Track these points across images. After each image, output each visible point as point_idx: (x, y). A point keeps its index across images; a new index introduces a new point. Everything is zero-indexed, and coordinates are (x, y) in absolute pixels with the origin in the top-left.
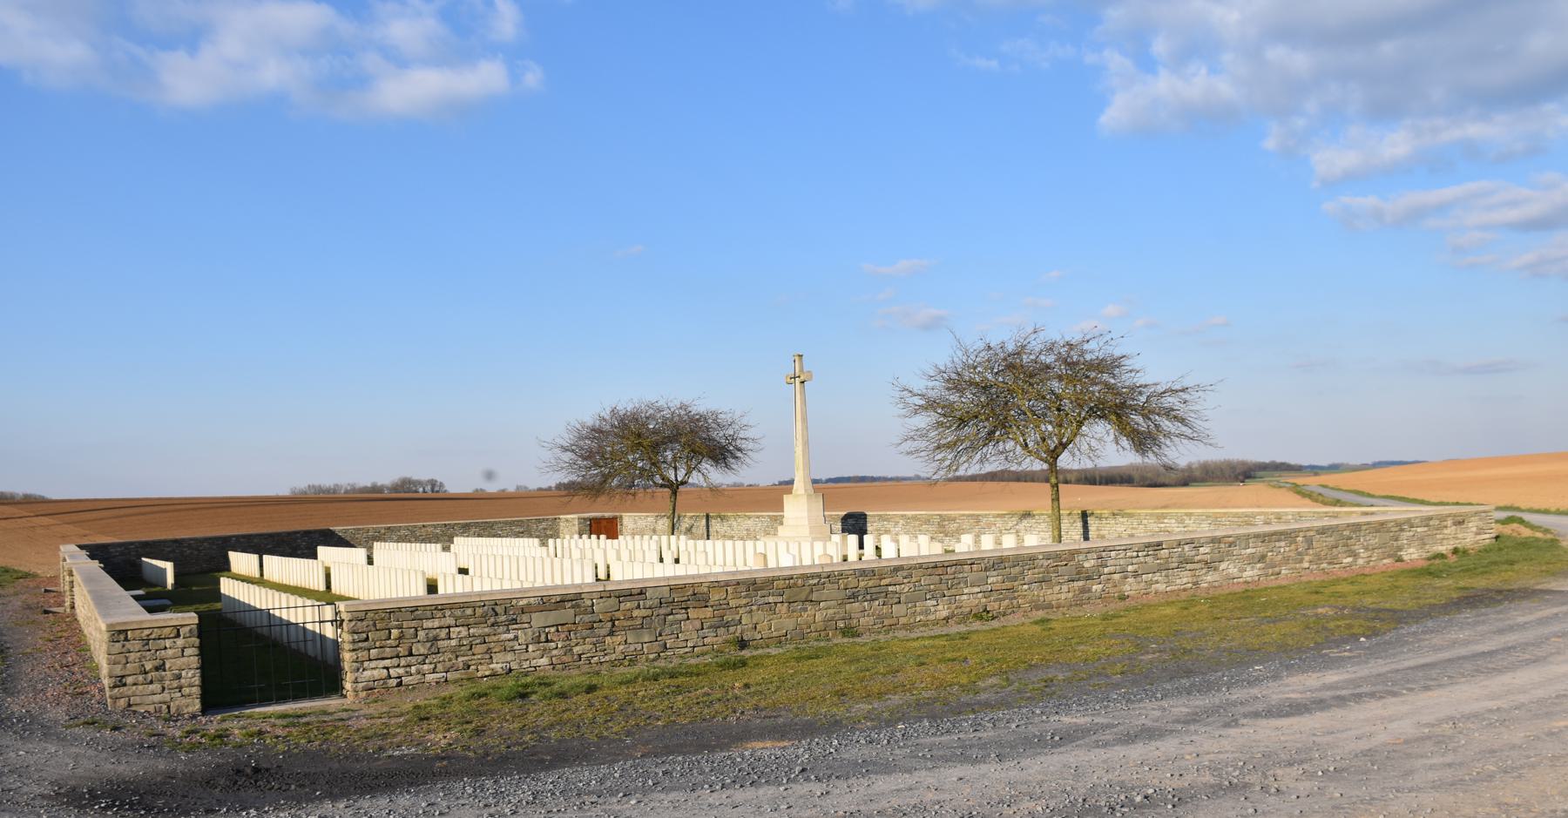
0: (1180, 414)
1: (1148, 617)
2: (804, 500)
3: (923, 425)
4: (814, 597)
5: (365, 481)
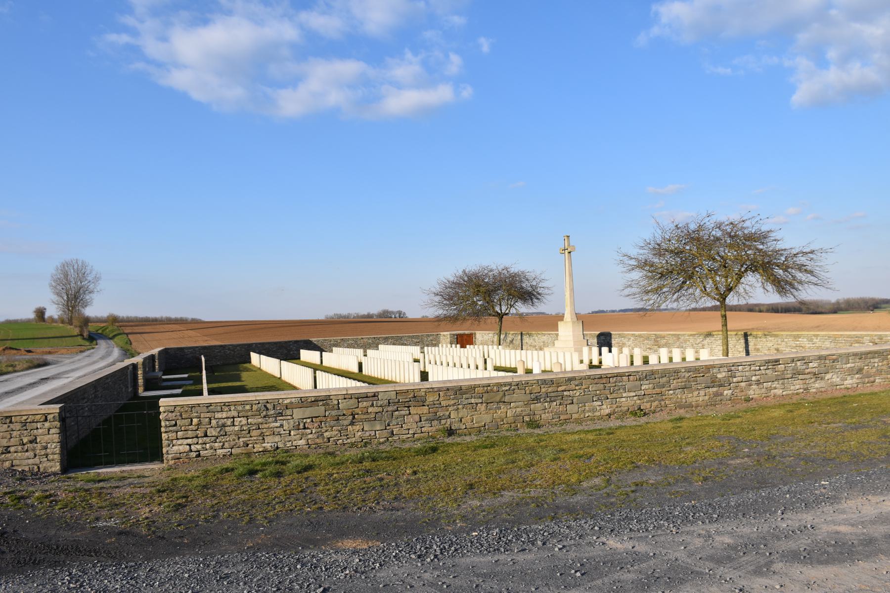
0: (809, 268)
1: (759, 418)
2: (570, 325)
3: (637, 278)
4: (507, 399)
5: (364, 311)
